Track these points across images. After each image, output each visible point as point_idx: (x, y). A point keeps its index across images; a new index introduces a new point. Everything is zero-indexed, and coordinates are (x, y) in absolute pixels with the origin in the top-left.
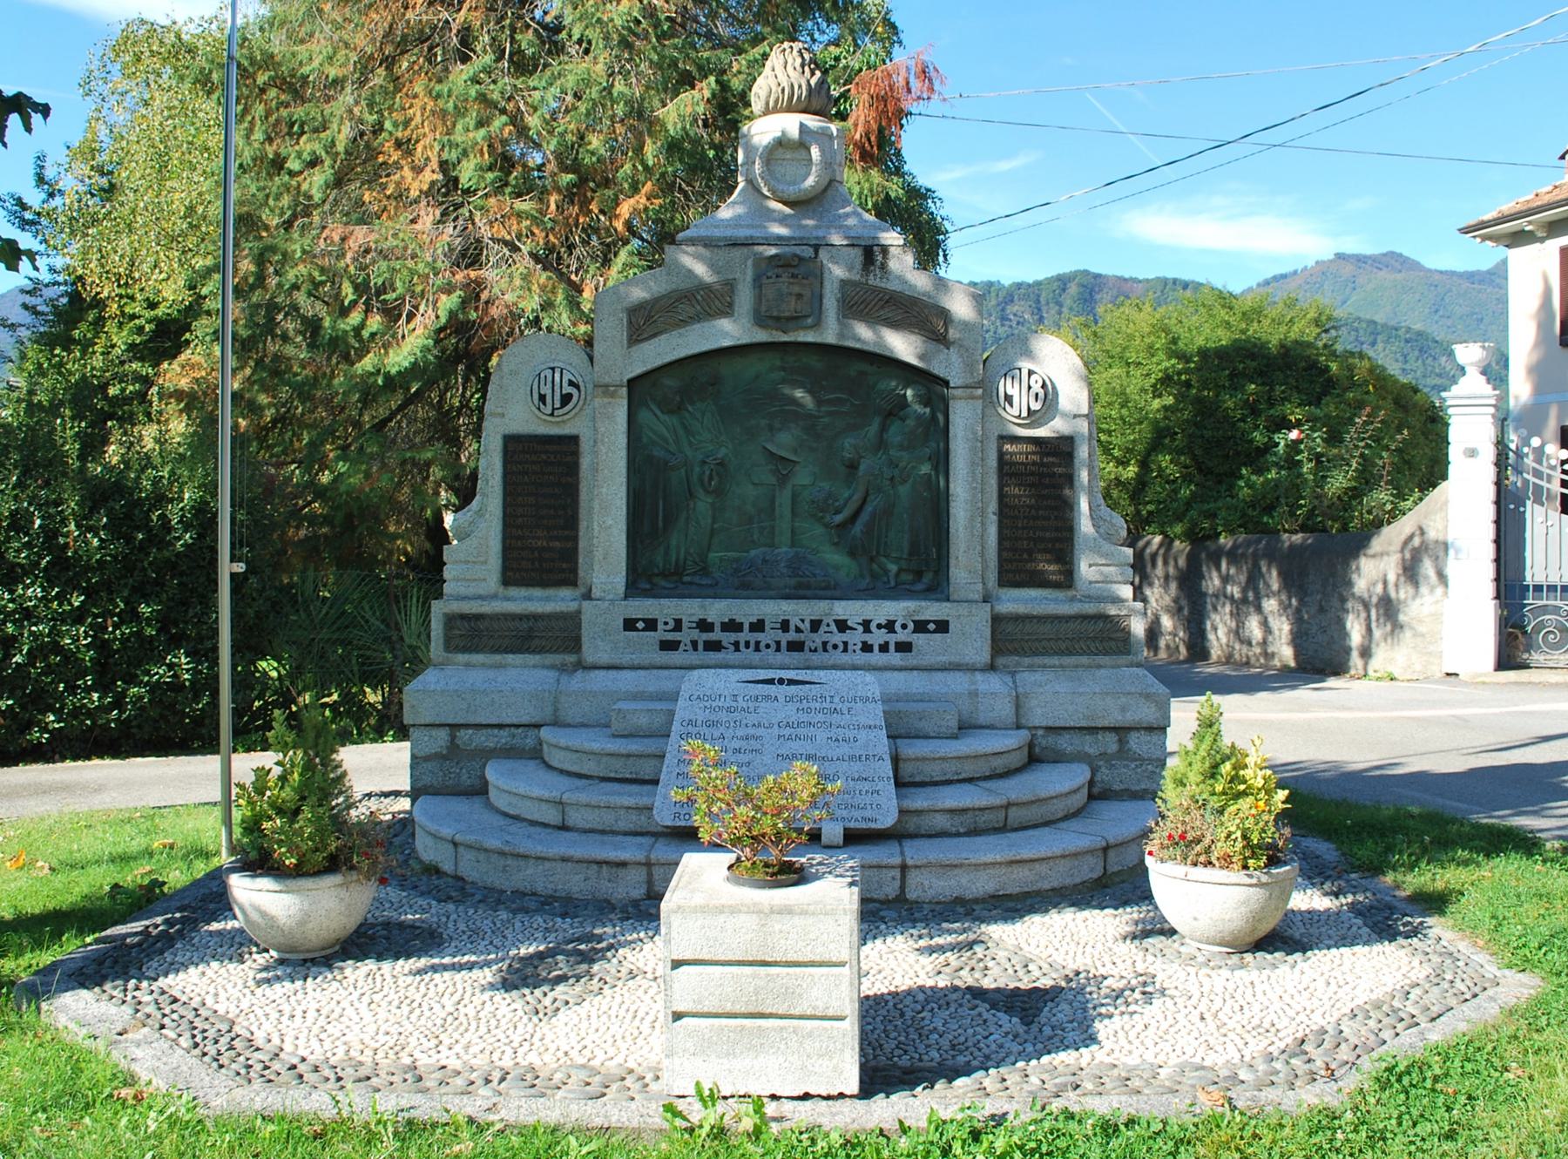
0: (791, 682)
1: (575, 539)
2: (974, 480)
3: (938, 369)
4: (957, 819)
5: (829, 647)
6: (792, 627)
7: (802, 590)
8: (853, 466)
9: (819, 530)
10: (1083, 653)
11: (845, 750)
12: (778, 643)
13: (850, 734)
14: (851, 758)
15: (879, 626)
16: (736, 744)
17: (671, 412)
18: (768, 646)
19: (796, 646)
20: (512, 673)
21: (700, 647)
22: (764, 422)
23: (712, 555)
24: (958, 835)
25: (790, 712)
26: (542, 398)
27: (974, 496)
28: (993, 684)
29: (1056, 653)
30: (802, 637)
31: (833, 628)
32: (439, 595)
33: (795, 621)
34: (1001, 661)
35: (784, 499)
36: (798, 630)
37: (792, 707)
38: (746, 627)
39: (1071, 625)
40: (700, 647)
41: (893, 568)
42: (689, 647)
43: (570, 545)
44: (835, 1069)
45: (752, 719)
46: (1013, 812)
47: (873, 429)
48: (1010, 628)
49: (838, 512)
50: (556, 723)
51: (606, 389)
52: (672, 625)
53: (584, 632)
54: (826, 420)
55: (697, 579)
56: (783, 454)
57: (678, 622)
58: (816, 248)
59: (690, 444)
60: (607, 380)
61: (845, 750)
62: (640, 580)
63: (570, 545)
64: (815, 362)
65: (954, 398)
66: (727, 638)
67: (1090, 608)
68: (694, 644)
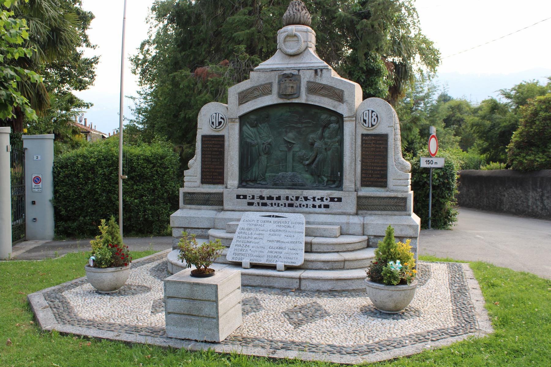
0: (277, 217)
1: (223, 169)
2: (352, 149)
3: (340, 111)
4: (326, 264)
5: (302, 206)
6: (290, 199)
7: (294, 186)
8: (312, 144)
9: (301, 166)
10: (389, 210)
11: (290, 239)
12: (285, 204)
13: (292, 234)
14: (291, 242)
15: (318, 199)
16: (255, 236)
17: (252, 127)
18: (282, 205)
19: (291, 205)
20: (203, 211)
21: (260, 204)
22: (284, 130)
23: (267, 174)
24: (326, 270)
25: (274, 226)
26: (213, 123)
27: (352, 155)
28: (357, 220)
29: (379, 210)
30: (292, 202)
31: (303, 199)
32: (182, 186)
33: (290, 197)
34: (360, 212)
35: (290, 156)
36: (292, 200)
37: (275, 225)
38: (275, 198)
39: (385, 200)
40: (260, 204)
41: (325, 179)
42: (257, 205)
43: (221, 170)
44: (213, 334)
45: (262, 228)
46: (347, 263)
47: (320, 132)
48: (364, 201)
49: (307, 160)
50: (214, 228)
51: (232, 120)
52: (251, 197)
53: (224, 199)
54: (304, 129)
55: (261, 182)
56: (290, 141)
57: (253, 198)
58: (299, 70)
59: (260, 138)
60: (232, 117)
61: (290, 239)
62: (244, 182)
63: (221, 170)
64: (300, 109)
65: (346, 121)
66: (269, 202)
67: (392, 194)
68: (258, 204)
